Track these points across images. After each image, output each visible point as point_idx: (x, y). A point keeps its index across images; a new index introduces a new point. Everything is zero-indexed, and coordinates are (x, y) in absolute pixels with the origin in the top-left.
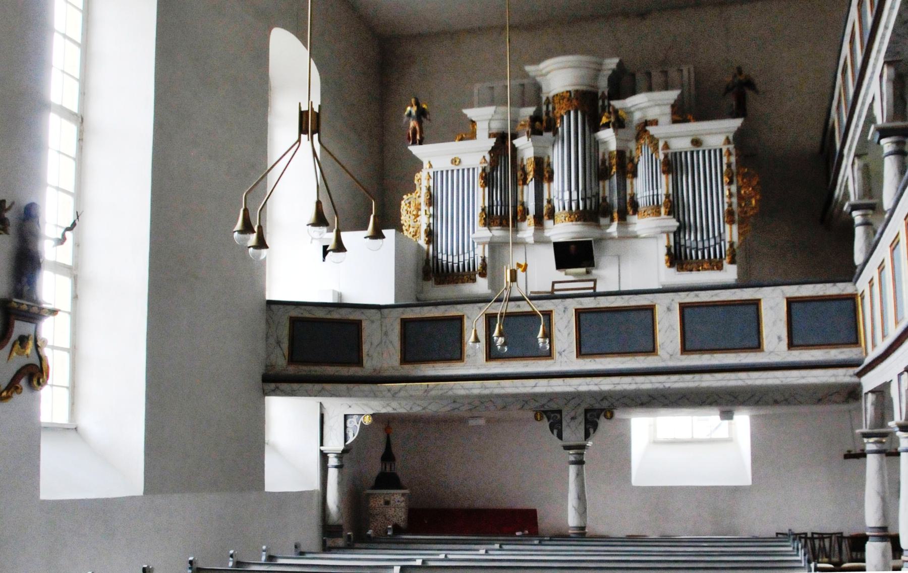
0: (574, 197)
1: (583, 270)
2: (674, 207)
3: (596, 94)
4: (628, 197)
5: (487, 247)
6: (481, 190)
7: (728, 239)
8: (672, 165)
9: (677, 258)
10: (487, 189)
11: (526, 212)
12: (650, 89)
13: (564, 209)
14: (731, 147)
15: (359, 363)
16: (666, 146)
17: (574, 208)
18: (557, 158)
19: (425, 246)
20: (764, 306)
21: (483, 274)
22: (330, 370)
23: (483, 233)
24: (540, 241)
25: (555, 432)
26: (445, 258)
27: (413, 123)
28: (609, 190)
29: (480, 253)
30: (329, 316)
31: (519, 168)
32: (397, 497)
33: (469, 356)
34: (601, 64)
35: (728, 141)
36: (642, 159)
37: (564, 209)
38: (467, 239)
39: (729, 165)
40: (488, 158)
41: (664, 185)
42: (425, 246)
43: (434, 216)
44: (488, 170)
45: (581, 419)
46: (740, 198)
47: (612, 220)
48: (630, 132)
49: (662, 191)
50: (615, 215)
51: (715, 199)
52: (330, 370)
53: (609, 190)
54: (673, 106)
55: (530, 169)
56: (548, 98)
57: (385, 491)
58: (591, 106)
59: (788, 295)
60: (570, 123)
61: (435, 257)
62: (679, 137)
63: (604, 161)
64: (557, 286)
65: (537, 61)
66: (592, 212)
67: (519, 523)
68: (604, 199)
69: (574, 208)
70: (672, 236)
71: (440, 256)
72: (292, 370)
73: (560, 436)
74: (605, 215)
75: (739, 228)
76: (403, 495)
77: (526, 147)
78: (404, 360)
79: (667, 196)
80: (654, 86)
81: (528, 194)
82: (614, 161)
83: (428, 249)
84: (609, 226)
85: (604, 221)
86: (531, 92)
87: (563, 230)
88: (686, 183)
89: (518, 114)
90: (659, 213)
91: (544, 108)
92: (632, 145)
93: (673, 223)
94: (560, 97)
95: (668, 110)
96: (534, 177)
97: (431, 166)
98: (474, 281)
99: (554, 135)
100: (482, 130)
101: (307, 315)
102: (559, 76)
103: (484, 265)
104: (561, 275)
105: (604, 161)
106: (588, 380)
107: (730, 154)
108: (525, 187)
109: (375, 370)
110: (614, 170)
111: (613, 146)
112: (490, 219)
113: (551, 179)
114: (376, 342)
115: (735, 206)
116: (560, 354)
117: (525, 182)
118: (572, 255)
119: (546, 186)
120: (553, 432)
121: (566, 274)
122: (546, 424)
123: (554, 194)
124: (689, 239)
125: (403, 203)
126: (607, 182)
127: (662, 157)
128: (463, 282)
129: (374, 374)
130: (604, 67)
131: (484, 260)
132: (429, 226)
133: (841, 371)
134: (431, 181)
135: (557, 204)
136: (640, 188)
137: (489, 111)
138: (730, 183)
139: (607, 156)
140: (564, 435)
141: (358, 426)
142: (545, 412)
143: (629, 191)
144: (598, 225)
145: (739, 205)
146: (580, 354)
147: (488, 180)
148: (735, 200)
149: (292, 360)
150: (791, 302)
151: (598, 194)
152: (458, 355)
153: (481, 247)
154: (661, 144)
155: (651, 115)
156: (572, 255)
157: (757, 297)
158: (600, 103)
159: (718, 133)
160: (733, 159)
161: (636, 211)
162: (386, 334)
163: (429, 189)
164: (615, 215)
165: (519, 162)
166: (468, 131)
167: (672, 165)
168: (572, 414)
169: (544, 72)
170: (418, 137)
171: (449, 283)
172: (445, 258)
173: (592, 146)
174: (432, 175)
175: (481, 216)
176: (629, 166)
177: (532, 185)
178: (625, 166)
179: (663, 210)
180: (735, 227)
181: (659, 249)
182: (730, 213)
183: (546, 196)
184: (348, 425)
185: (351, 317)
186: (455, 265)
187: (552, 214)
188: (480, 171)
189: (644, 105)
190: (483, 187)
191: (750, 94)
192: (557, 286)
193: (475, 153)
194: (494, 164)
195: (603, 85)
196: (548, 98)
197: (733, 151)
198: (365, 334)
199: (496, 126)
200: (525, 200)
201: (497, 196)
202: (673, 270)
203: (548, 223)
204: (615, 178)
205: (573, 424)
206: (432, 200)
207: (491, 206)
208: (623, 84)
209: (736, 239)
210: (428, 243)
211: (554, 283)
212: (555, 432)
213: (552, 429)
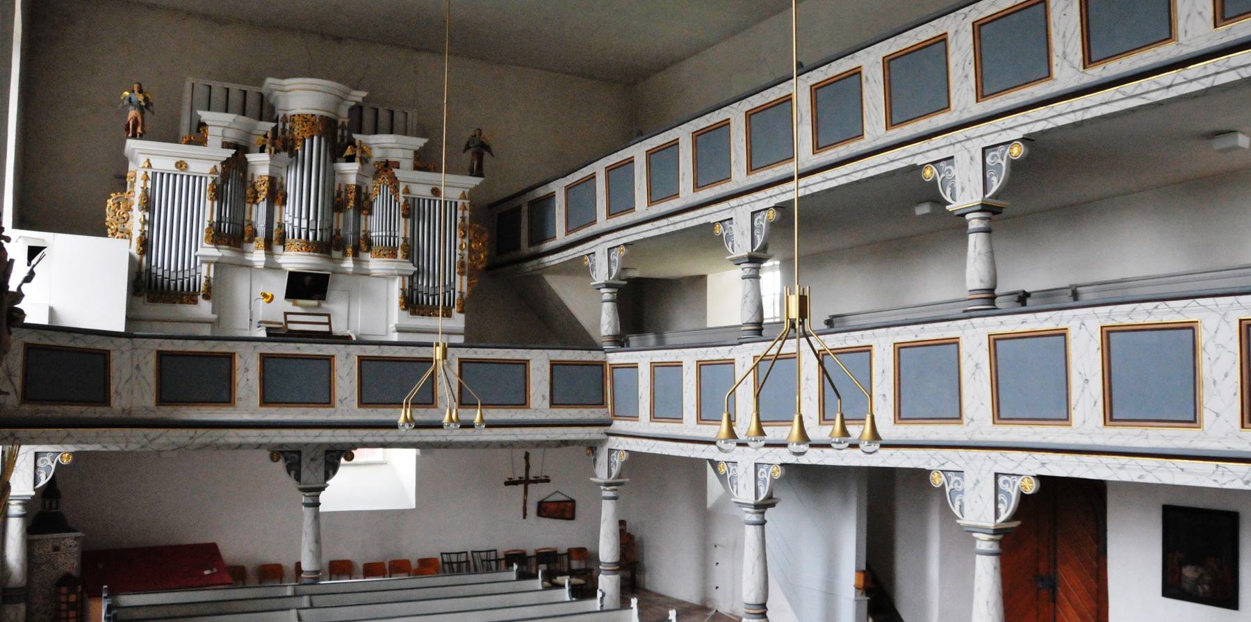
0: (312, 226)
1: (315, 303)
2: (411, 251)
3: (335, 122)
4: (362, 234)
5: (212, 267)
6: (209, 203)
7: (457, 289)
8: (411, 210)
9: (411, 303)
10: (216, 203)
11: (255, 233)
12: (391, 131)
13: (300, 237)
14: (467, 202)
15: (106, 401)
16: (407, 191)
17: (311, 238)
18: (292, 181)
19: (138, 257)
20: (532, 365)
21: (206, 297)
22: (74, 411)
23: (210, 251)
24: (272, 267)
25: (293, 473)
26: (160, 272)
27: (133, 113)
28: (344, 223)
29: (204, 271)
30: (72, 344)
31: (249, 184)
32: (69, 541)
33: (240, 399)
34: (348, 94)
35: (463, 196)
36: (380, 198)
37: (300, 237)
38: (192, 254)
39: (463, 218)
40: (219, 169)
41: (402, 229)
42: (138, 257)
43: (150, 223)
44: (219, 182)
45: (321, 460)
46: (471, 251)
47: (345, 254)
48: (371, 168)
49: (401, 234)
50: (350, 250)
51: (451, 252)
52: (74, 411)
53: (344, 223)
54: (416, 152)
55: (263, 189)
56: (285, 116)
57: (55, 536)
58: (337, 137)
59: (553, 358)
60: (313, 148)
61: (149, 270)
62: (419, 184)
63: (339, 194)
64: (290, 318)
65: (285, 73)
66: (328, 245)
67: (195, 563)
68: (338, 232)
69: (311, 238)
70: (407, 279)
71: (154, 270)
72: (28, 410)
73: (298, 478)
74: (337, 249)
75: (469, 280)
76: (76, 538)
77: (260, 164)
78: (161, 400)
79: (405, 239)
80: (395, 128)
81: (258, 214)
82: (352, 196)
83: (141, 261)
84: (341, 260)
85: (337, 254)
86: (265, 109)
87: (294, 260)
88: (422, 228)
89: (255, 127)
90: (394, 255)
91: (280, 126)
92: (369, 182)
93: (411, 268)
94: (305, 119)
95: (411, 154)
96: (267, 196)
97: (150, 166)
98: (195, 302)
99: (291, 156)
100: (215, 136)
101: (46, 342)
102: (301, 97)
103: (209, 288)
104: (289, 306)
105: (339, 194)
106: (375, 431)
107: (464, 209)
108: (254, 206)
109: (124, 410)
110: (352, 204)
111: (352, 180)
112: (217, 236)
113: (284, 203)
114: (126, 376)
115: (466, 259)
116: (341, 401)
117: (255, 200)
118: (304, 287)
119: (277, 208)
120: (289, 473)
121: (295, 304)
122: (281, 465)
123: (287, 218)
124: (423, 283)
125: (110, 202)
126: (341, 215)
127: (402, 200)
128: (182, 303)
129: (124, 416)
130: (350, 98)
131: (208, 280)
132: (143, 234)
133: (596, 429)
134: (149, 184)
135: (288, 229)
136: (375, 226)
137: (229, 118)
138: (464, 237)
139: (343, 189)
140: (304, 477)
141: (53, 466)
142: (282, 452)
143: (363, 228)
144: (332, 259)
145: (470, 257)
146: (362, 403)
147: (218, 193)
148: (466, 253)
149: (26, 398)
150: (554, 364)
151: (331, 227)
152: (226, 397)
153: (205, 266)
154: (402, 187)
155: (394, 156)
156: (304, 287)
157: (527, 357)
158: (339, 132)
159: (455, 187)
160: (467, 214)
161: (369, 249)
162: (138, 367)
163: (145, 191)
164: (350, 250)
165: (249, 178)
166: (198, 135)
167: (411, 210)
168: (312, 455)
169: (287, 88)
170: (139, 130)
171: (164, 301)
172: (160, 272)
173: (331, 175)
174: (150, 175)
175: (208, 231)
176: (366, 204)
177: (263, 206)
178: (363, 204)
179: (399, 252)
180: (465, 278)
181: (395, 290)
182: (462, 264)
183: (277, 219)
184: (40, 464)
185: (99, 346)
186: (172, 283)
187: (283, 240)
188: (210, 181)
189: (383, 145)
190: (212, 199)
191: (486, 155)
192: (290, 318)
193: (205, 161)
194: (225, 176)
195: (344, 116)
196: (285, 116)
197: (468, 206)
198: (114, 365)
199: (231, 136)
200: (253, 219)
201: (227, 212)
202: (406, 313)
203: (278, 249)
204: (351, 212)
205: (313, 465)
206: (148, 205)
207: (219, 221)
208: (360, 119)
209: (465, 289)
210: (142, 253)
211: (286, 314)
212: (293, 473)
213: (289, 469)
